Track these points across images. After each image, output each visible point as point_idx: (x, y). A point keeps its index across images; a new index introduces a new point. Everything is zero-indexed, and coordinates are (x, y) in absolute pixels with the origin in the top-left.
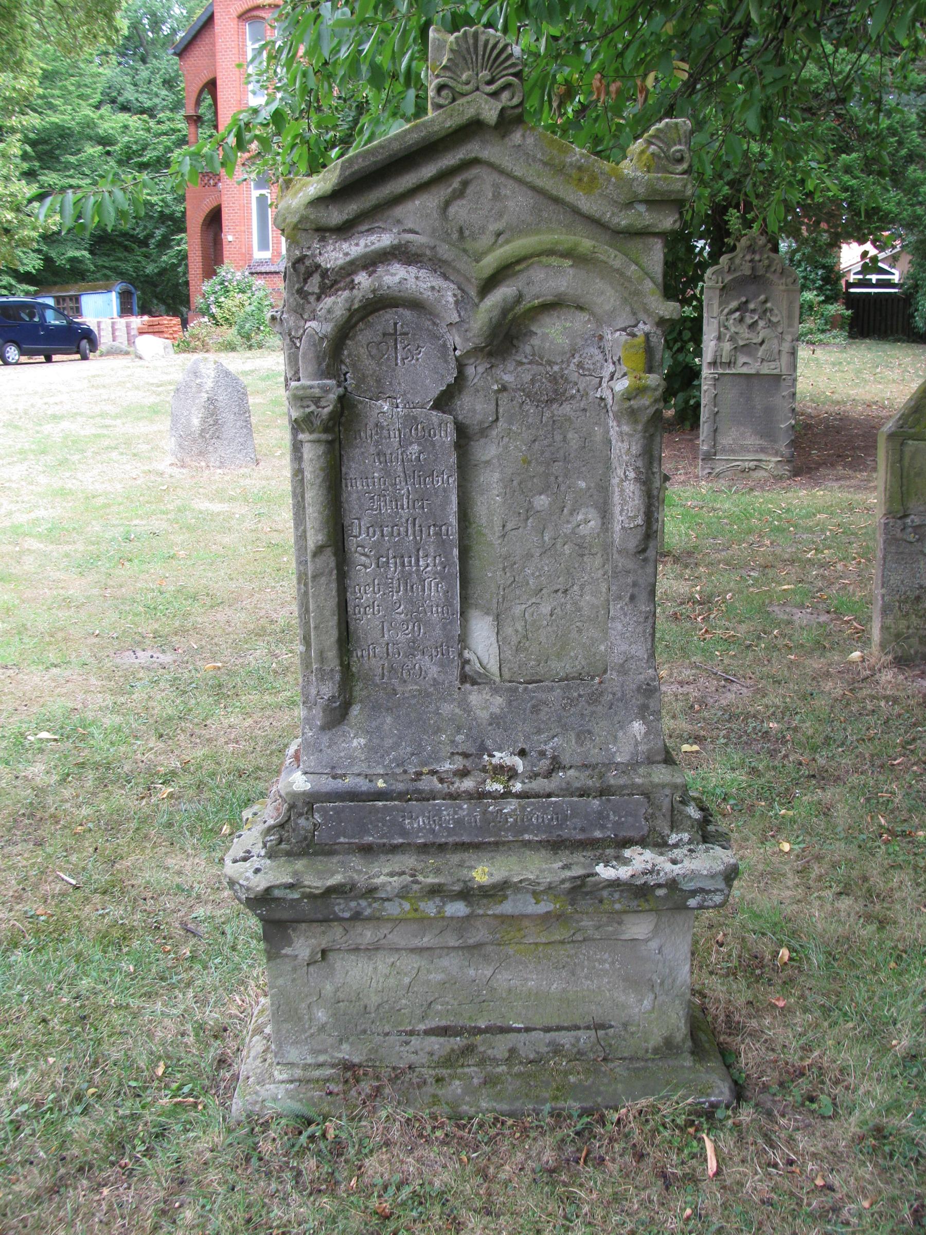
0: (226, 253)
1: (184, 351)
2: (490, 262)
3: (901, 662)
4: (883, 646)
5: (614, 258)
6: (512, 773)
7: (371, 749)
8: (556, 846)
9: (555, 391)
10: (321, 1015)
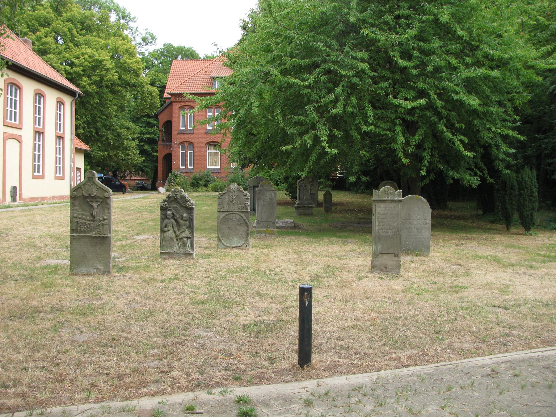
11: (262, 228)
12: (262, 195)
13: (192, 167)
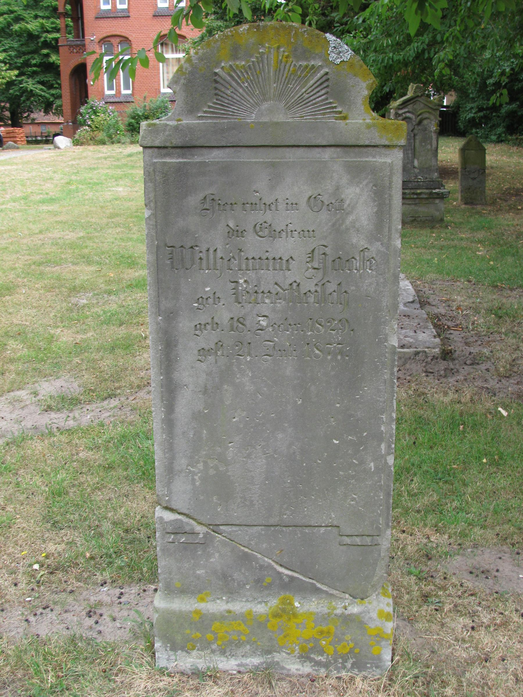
0: (90, 91)
1: (77, 145)
2: (419, 113)
3: (466, 204)
4: (461, 200)
5: (434, 112)
8: (427, 189)
9: (425, 129)
11: (229, 588)
12: (212, 206)
13: (129, 92)
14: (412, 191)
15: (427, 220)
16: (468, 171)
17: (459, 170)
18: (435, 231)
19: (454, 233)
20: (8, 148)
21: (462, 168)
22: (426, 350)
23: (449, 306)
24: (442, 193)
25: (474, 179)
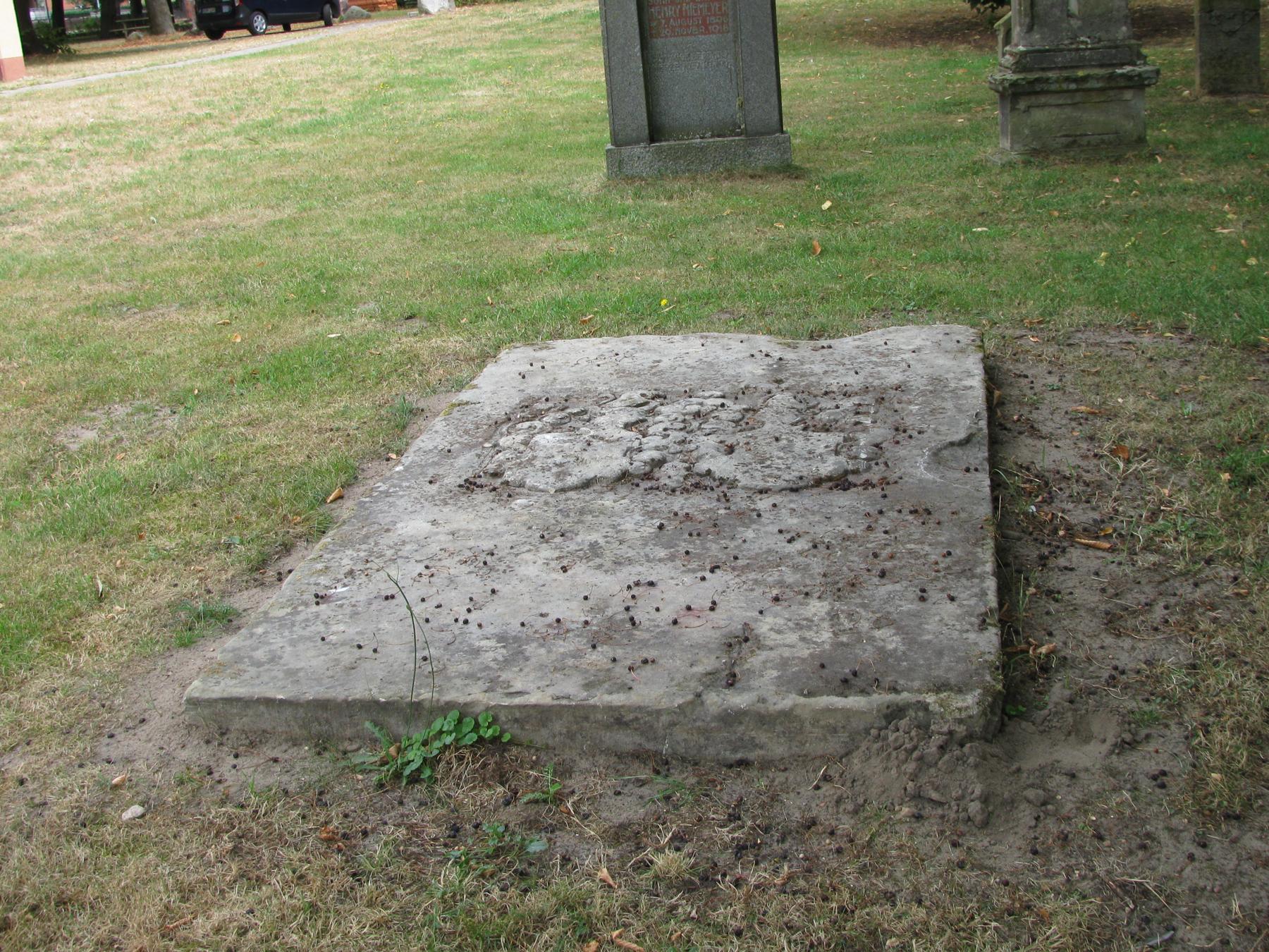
1: (464, 5)
3: (1212, 93)
4: (1202, 85)
6: (1086, 43)
7: (1042, 38)
8: (1101, 66)
10: (1026, 131)
14: (1065, 74)
15: (1103, 142)
16: (1218, 17)
17: (1196, 14)
18: (1122, 168)
19: (1169, 171)
20: (351, 18)
21: (1202, 10)
22: (930, 699)
23: (1092, 438)
24: (1139, 75)
25: (1231, 34)
